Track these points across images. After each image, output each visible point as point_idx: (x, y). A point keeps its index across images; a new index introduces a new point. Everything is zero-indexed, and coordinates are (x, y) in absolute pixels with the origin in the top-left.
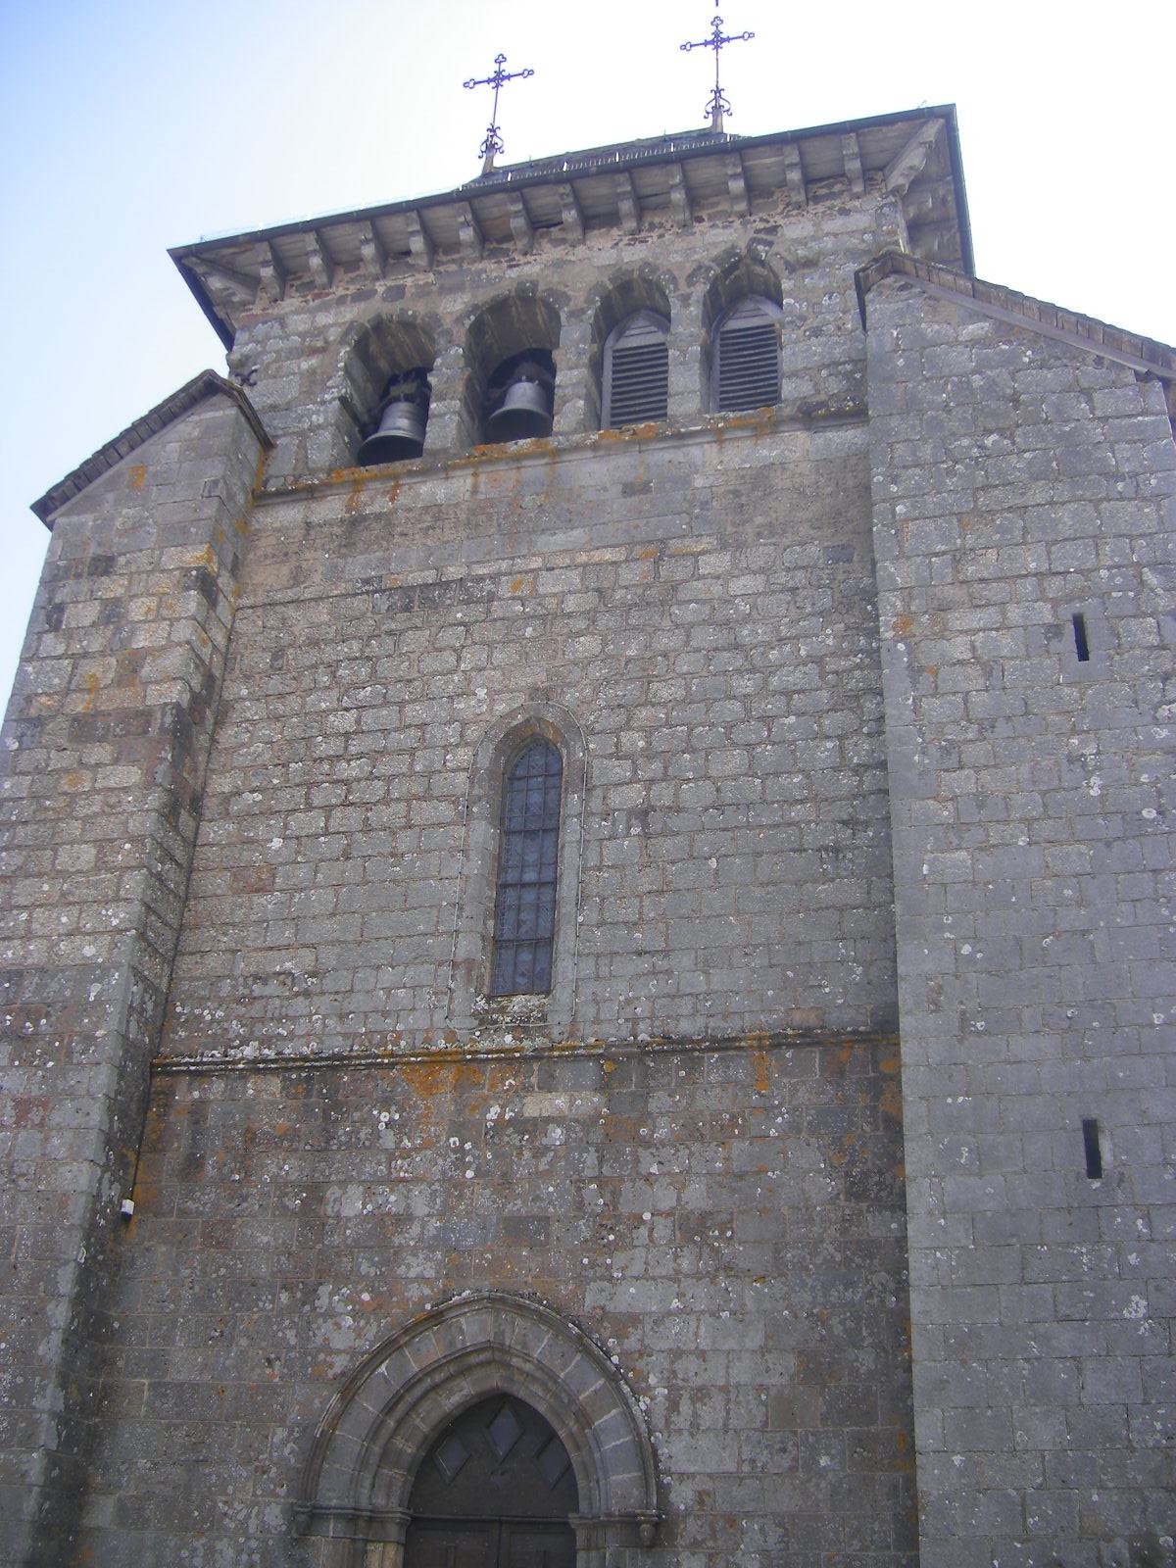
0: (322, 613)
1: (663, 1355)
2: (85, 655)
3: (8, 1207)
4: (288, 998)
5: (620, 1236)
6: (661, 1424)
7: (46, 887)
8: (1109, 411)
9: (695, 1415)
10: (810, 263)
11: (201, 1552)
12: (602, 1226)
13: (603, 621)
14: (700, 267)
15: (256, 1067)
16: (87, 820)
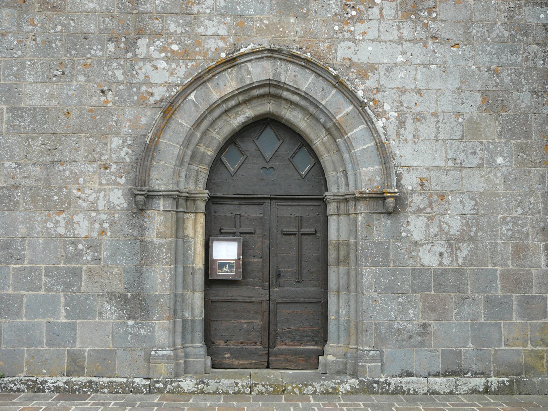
1: (393, 91)
5: (360, 12)
6: (394, 136)
9: (416, 130)
11: (62, 223)
12: (347, 5)
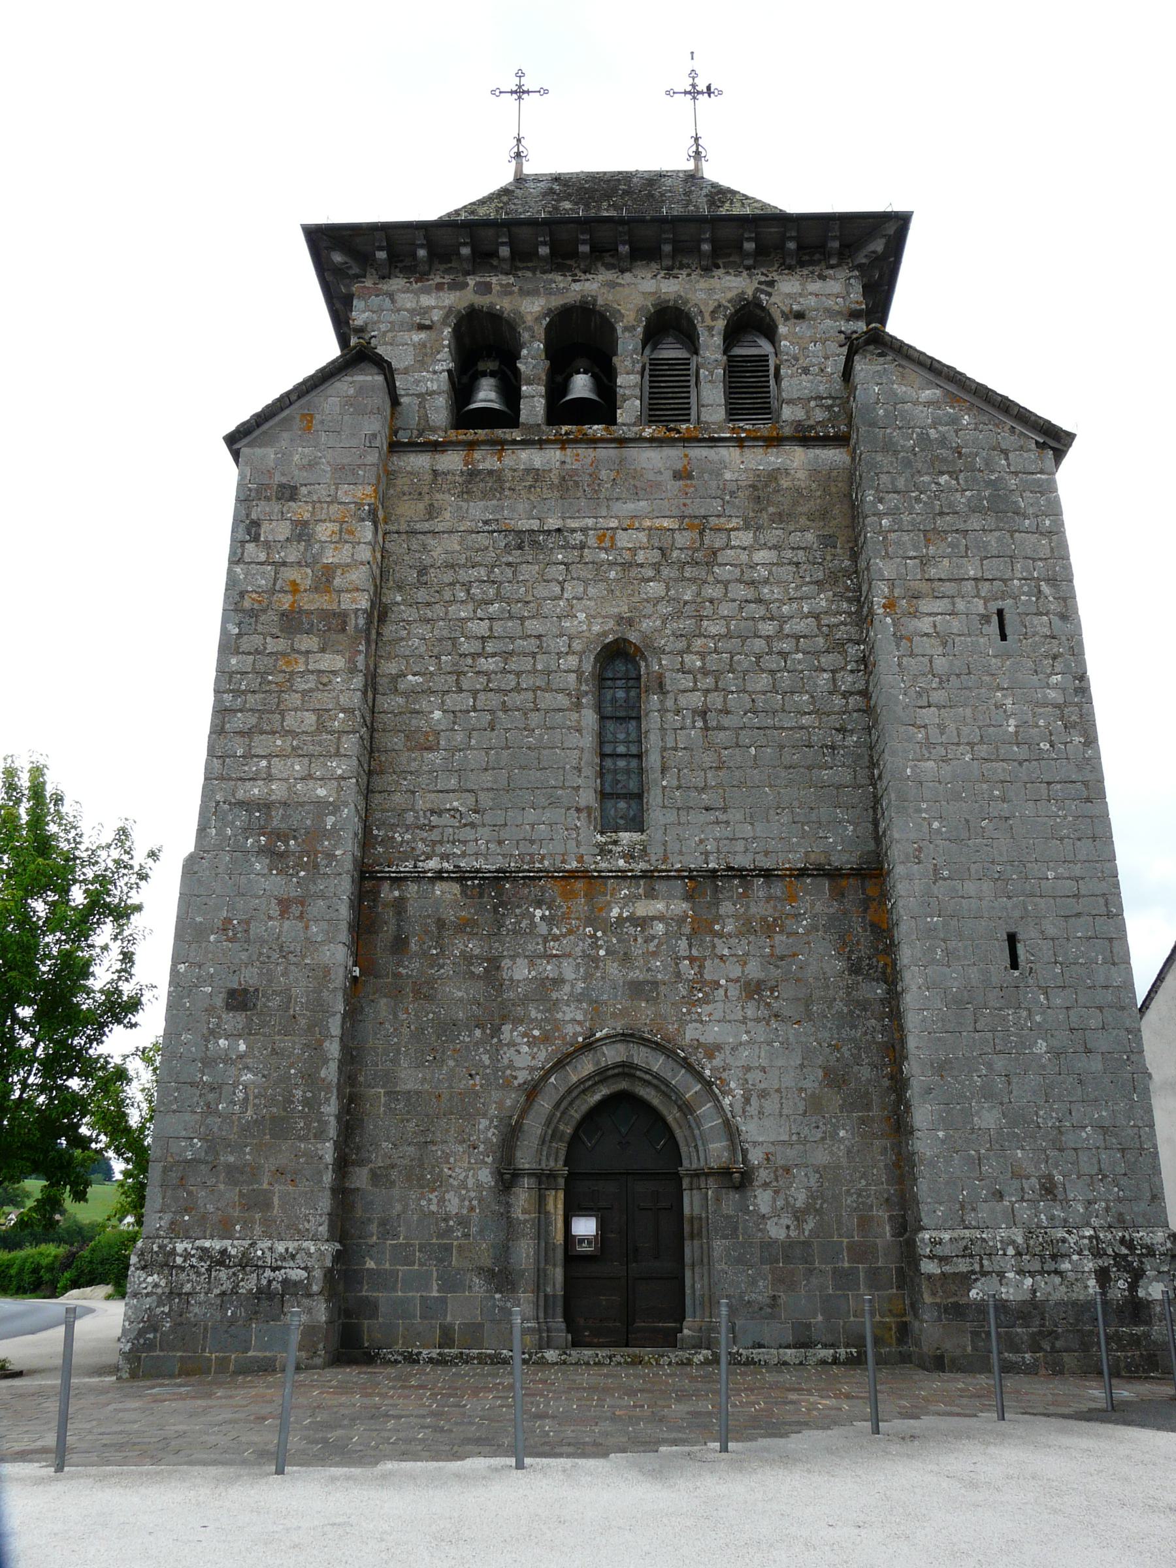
0: (453, 542)
2: (284, 564)
3: (282, 975)
4: (458, 828)
5: (706, 994)
7: (279, 742)
8: (1020, 468)
9: (761, 1107)
10: (800, 316)
11: (435, 1201)
13: (666, 571)
14: (720, 306)
15: (439, 876)
16: (304, 693)
